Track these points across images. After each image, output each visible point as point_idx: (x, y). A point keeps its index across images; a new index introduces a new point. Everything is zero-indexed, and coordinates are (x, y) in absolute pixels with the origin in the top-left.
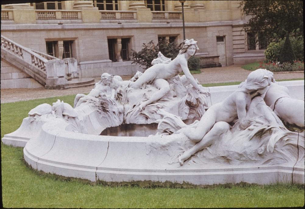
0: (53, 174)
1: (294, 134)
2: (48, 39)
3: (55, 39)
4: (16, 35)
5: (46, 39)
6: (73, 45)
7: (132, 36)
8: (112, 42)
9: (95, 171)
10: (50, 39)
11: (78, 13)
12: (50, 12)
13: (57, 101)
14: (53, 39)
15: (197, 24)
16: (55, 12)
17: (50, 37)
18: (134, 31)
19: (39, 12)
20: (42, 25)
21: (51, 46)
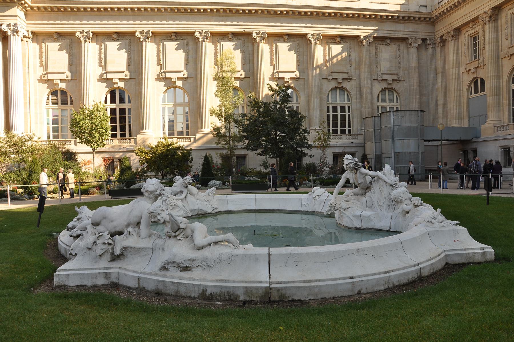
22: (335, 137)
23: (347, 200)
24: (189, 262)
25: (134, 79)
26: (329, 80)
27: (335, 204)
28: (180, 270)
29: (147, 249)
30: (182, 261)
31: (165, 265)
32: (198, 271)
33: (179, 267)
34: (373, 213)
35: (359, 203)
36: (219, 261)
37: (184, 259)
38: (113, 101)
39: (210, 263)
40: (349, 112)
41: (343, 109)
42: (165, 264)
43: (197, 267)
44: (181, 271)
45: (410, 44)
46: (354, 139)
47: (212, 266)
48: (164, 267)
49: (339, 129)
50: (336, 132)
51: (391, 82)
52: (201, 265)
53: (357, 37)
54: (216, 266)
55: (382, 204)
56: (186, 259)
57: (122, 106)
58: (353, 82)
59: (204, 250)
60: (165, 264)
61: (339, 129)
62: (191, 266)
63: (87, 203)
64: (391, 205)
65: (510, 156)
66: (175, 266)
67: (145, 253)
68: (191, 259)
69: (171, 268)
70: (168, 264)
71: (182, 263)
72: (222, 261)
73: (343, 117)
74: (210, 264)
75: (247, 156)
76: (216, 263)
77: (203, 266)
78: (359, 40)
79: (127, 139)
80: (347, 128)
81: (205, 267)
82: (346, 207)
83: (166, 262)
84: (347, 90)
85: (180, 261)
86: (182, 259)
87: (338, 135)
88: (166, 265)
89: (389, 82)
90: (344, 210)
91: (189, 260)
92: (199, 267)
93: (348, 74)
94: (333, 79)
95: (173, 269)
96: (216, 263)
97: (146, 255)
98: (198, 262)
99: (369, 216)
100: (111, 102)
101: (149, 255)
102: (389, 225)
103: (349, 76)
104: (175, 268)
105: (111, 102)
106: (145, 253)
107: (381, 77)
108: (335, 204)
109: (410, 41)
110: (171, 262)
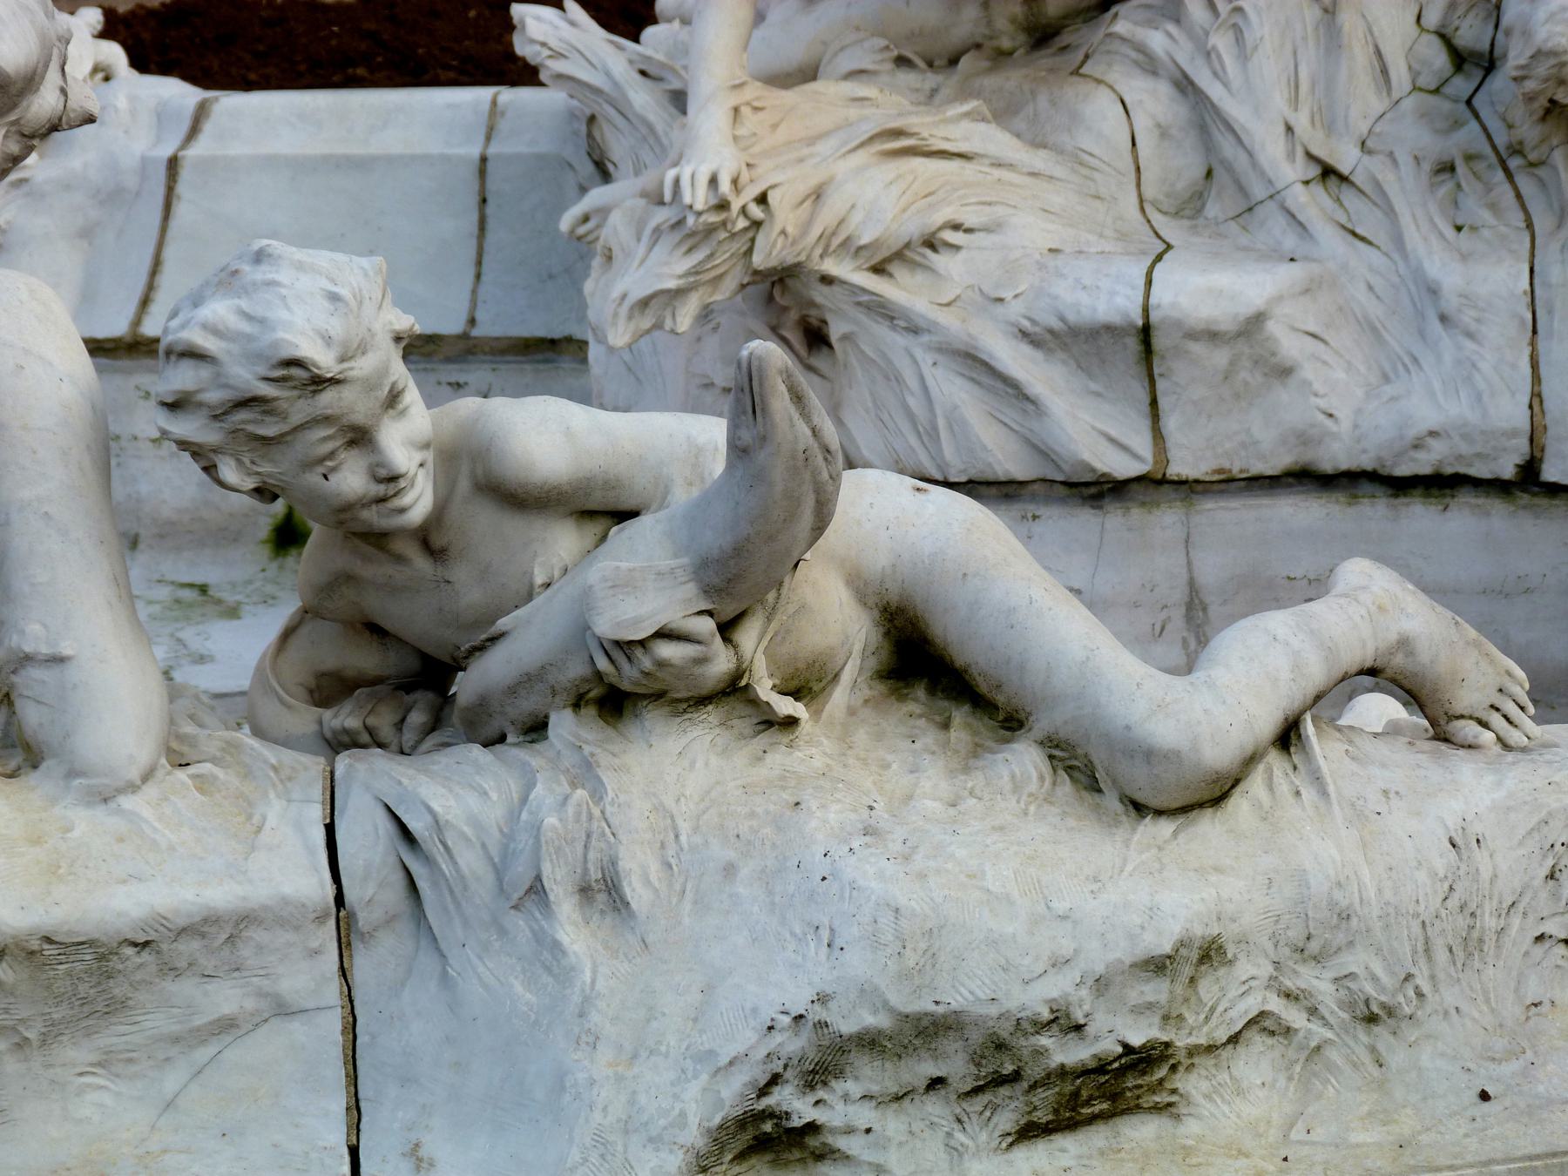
23: (898, 133)
24: (1156, 990)
27: (762, 199)
28: (1007, 1120)
29: (257, 935)
30: (1057, 987)
31: (763, 1092)
32: (1240, 1092)
33: (1016, 1077)
34: (1284, 276)
35: (1039, 160)
36: (1462, 922)
37: (1097, 959)
39: (1378, 968)
42: (775, 1080)
43: (1234, 1039)
44: (1028, 1132)
47: (1405, 1002)
48: (746, 1121)
52: (1275, 1004)
54: (1450, 996)
55: (1346, 157)
56: (1123, 952)
59: (1240, 805)
60: (775, 1080)
62: (1182, 1041)
64: (1469, 158)
66: (936, 1083)
67: (226, 998)
68: (1182, 944)
69: (864, 1115)
70: (818, 1075)
71: (1067, 1024)
72: (1490, 922)
74: (1378, 982)
76: (1441, 956)
77: (1295, 1017)
81: (1319, 1032)
82: (912, 227)
83: (793, 1044)
85: (1035, 999)
86: (1059, 963)
88: (775, 1099)
90: (878, 270)
91: (1158, 966)
92: (1257, 1042)
95: (892, 1124)
96: (1441, 956)
97: (226, 1026)
98: (1244, 969)
99: (1254, 324)
101: (283, 1010)
102: (1512, 412)
104: (935, 1107)
106: (226, 998)
108: (762, 199)
110: (870, 1042)
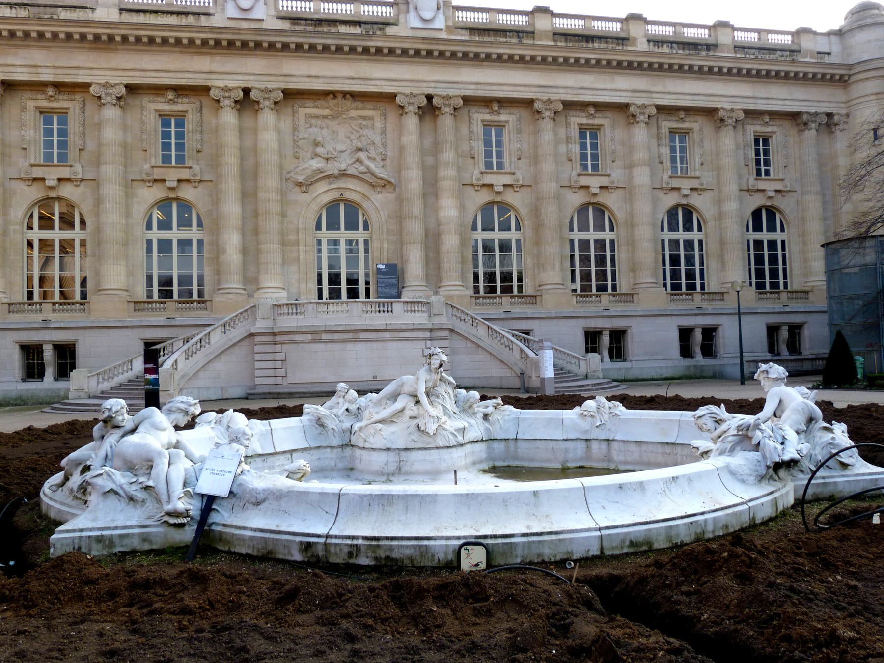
0: (385, 558)
1: (407, 499)
2: (588, 328)
3: (598, 328)
4: (501, 322)
5: (584, 328)
6: (626, 335)
7: (720, 325)
8: (685, 334)
9: (598, 533)
10: (590, 328)
11: (634, 296)
12: (774, 293)
13: (719, 407)
14: (595, 328)
15: (62, 325)
16: (779, 292)
17: (589, 326)
18: (725, 317)
19: (760, 293)
20: (582, 310)
21: (592, 339)
22: (184, 305)
25: (529, 188)
26: (476, 188)
38: (46, 223)
40: (783, 249)
41: (600, 244)
45: (806, 124)
46: (530, 303)
49: (683, 282)
50: (492, 290)
51: (773, 194)
53: (625, 108)
57: (772, 236)
58: (708, 195)
61: (683, 282)
63: (726, 400)
65: (42, 360)
73: (601, 260)
75: (629, 331)
78: (628, 114)
79: (194, 301)
80: (698, 282)
84: (512, 207)
87: (681, 294)
89: (496, 189)
93: (611, 178)
94: (484, 185)
100: (754, 231)
103: (613, 182)
105: (754, 231)
107: (668, 183)
109: (805, 117)
